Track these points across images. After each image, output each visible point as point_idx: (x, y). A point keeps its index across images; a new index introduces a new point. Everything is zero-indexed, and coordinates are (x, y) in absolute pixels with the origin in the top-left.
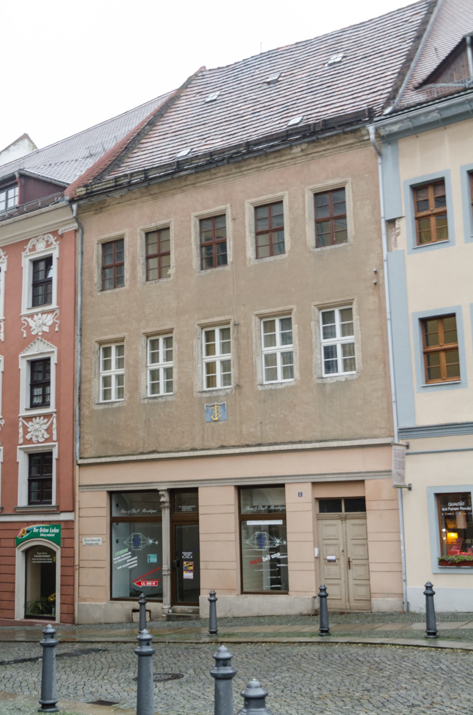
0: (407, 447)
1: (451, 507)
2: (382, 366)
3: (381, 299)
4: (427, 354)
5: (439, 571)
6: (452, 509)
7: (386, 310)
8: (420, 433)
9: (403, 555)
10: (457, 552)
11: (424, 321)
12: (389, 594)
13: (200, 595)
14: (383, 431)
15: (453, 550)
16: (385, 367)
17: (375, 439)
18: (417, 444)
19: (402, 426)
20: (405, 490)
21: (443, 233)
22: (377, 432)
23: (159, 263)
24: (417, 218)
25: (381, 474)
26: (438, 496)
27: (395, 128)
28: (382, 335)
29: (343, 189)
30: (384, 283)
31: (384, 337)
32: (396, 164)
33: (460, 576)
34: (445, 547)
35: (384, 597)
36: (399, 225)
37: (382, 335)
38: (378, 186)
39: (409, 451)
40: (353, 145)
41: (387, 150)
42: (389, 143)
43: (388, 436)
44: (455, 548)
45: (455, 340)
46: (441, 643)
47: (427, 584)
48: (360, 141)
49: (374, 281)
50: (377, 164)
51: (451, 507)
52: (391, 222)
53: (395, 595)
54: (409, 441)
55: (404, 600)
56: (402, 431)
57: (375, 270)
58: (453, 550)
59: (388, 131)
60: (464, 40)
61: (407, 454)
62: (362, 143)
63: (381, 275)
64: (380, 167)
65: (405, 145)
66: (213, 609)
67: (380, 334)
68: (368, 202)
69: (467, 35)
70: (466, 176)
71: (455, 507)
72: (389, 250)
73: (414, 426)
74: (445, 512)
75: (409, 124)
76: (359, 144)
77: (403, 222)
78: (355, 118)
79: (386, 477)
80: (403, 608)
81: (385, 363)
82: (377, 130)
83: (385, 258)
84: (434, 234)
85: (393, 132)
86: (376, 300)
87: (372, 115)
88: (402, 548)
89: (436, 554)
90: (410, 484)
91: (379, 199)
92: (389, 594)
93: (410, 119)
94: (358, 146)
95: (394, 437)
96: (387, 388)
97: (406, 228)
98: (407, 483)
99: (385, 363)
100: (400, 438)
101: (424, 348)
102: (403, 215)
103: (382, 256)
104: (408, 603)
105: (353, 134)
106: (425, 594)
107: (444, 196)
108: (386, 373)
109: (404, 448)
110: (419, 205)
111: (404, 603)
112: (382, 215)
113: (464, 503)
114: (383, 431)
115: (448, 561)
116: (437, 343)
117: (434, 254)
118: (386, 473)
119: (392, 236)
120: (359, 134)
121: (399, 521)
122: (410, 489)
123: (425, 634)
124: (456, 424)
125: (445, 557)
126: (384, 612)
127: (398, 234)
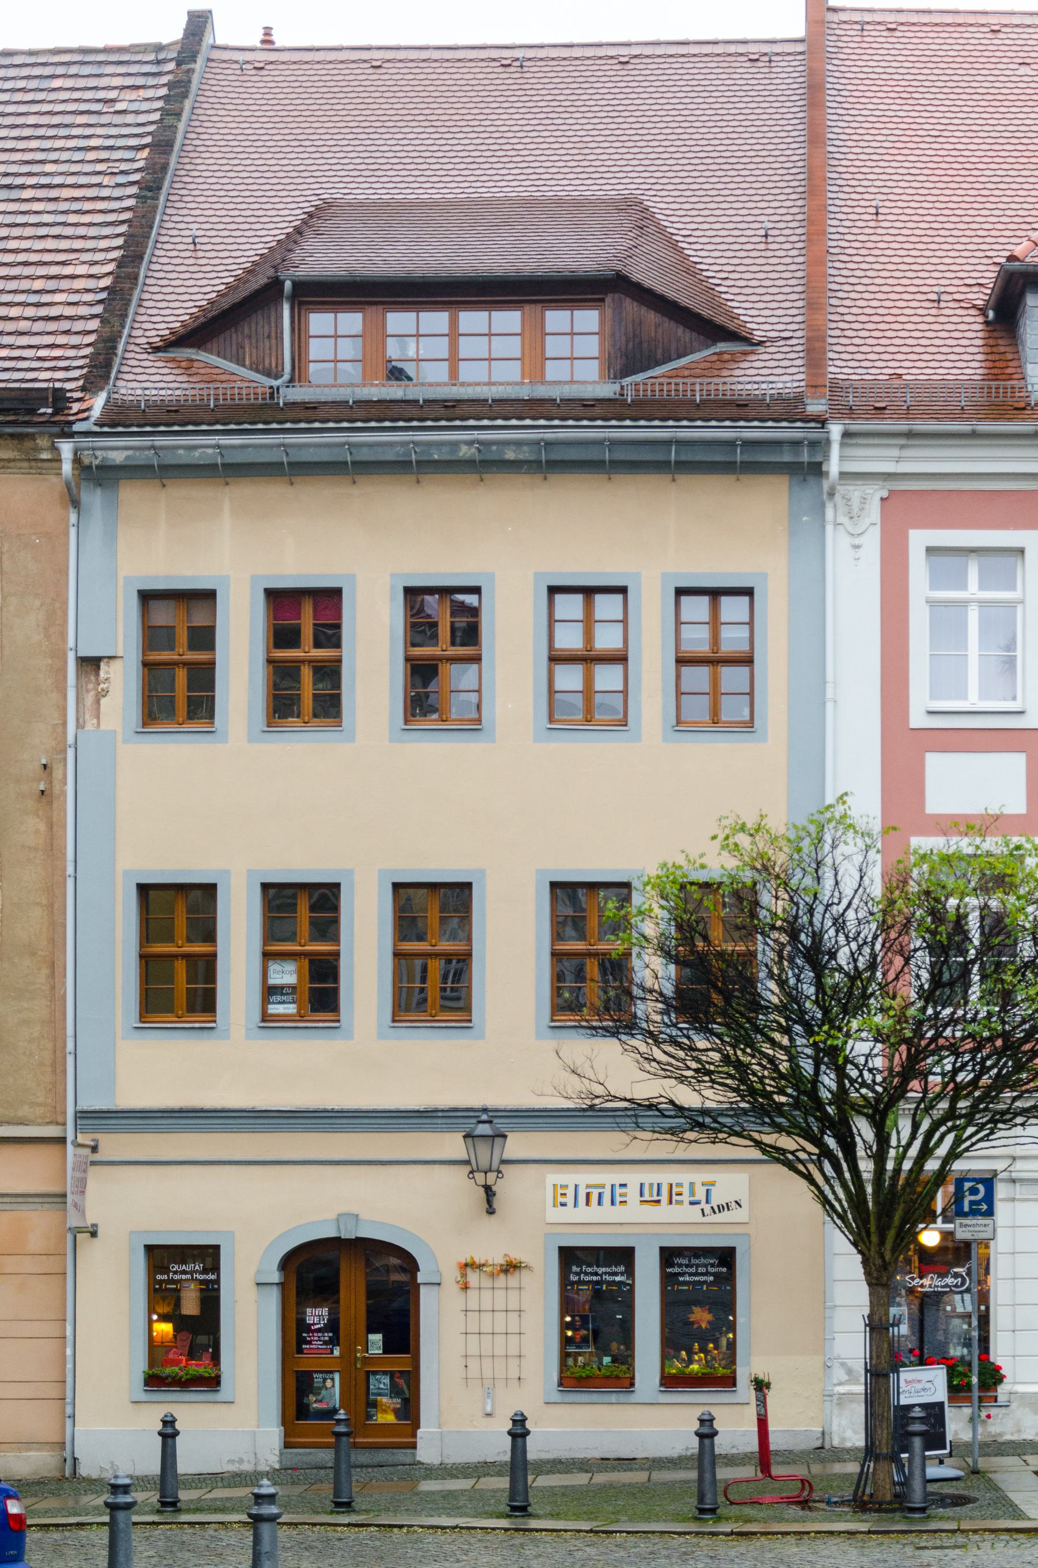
0: (94, 1149)
1: (175, 1273)
2: (45, 971)
3: (53, 829)
4: (146, 959)
5: (144, 1397)
6: (177, 1277)
7: (65, 854)
8: (123, 1122)
9: (69, 1366)
10: (181, 1361)
11: (144, 889)
12: (29, 1445)
14: (39, 1111)
15: (171, 1356)
16: (52, 975)
17: (21, 1127)
18: (115, 1144)
19: (85, 1105)
22: (24, 1111)
24: (145, 664)
25: (30, 1200)
26: (150, 1249)
28: (51, 905)
30: (64, 793)
31: (54, 910)
32: (111, 538)
33: (187, 1405)
34: (155, 1348)
35: (20, 1450)
36: (107, 672)
37: (51, 905)
39: (97, 1157)
40: (12, 464)
41: (93, 498)
42: (99, 484)
43: (48, 1123)
44: (175, 1353)
45: (210, 936)
47: (166, 1416)
48: (29, 460)
49: (42, 787)
51: (175, 1273)
52: (90, 664)
53: (42, 1445)
54: (98, 1136)
55: (67, 1454)
56: (82, 1115)
57: (44, 761)
58: (171, 1356)
59: (100, 458)
61: (93, 1163)
62: (33, 464)
63: (57, 774)
64: (73, 531)
65: (132, 495)
67: (45, 902)
68: (37, 603)
70: (261, 597)
71: (184, 1272)
72: (80, 725)
73: (112, 1107)
74: (161, 1282)
76: (26, 464)
77: (116, 667)
78: (22, 401)
79: (39, 1206)
80: (64, 1470)
81: (52, 965)
83: (70, 739)
85: (110, 463)
86: (42, 827)
87: (60, 405)
88: (69, 1352)
89: (141, 1365)
90: (94, 1225)
91: (66, 602)
92: (29, 1445)
94: (21, 468)
95: (64, 1124)
96: (55, 1022)
97: (122, 682)
98: (89, 1222)
99: (52, 965)
101: (141, 946)
102: (120, 654)
103: (65, 738)
104: (75, 1459)
105: (15, 442)
106: (160, 1434)
107: (211, 630)
108: (53, 988)
109: (88, 1151)
110: (153, 637)
111: (65, 1460)
112: (71, 643)
113: (693, 1318)
114: (39, 1111)
115: (167, 1378)
116: (170, 939)
117: (177, 751)
118: (40, 1200)
119: (88, 691)
120: (28, 444)
121: (65, 1299)
122: (94, 1234)
123: (158, 1506)
124: (202, 1111)
125: (157, 1371)
126: (20, 1481)
127: (105, 693)
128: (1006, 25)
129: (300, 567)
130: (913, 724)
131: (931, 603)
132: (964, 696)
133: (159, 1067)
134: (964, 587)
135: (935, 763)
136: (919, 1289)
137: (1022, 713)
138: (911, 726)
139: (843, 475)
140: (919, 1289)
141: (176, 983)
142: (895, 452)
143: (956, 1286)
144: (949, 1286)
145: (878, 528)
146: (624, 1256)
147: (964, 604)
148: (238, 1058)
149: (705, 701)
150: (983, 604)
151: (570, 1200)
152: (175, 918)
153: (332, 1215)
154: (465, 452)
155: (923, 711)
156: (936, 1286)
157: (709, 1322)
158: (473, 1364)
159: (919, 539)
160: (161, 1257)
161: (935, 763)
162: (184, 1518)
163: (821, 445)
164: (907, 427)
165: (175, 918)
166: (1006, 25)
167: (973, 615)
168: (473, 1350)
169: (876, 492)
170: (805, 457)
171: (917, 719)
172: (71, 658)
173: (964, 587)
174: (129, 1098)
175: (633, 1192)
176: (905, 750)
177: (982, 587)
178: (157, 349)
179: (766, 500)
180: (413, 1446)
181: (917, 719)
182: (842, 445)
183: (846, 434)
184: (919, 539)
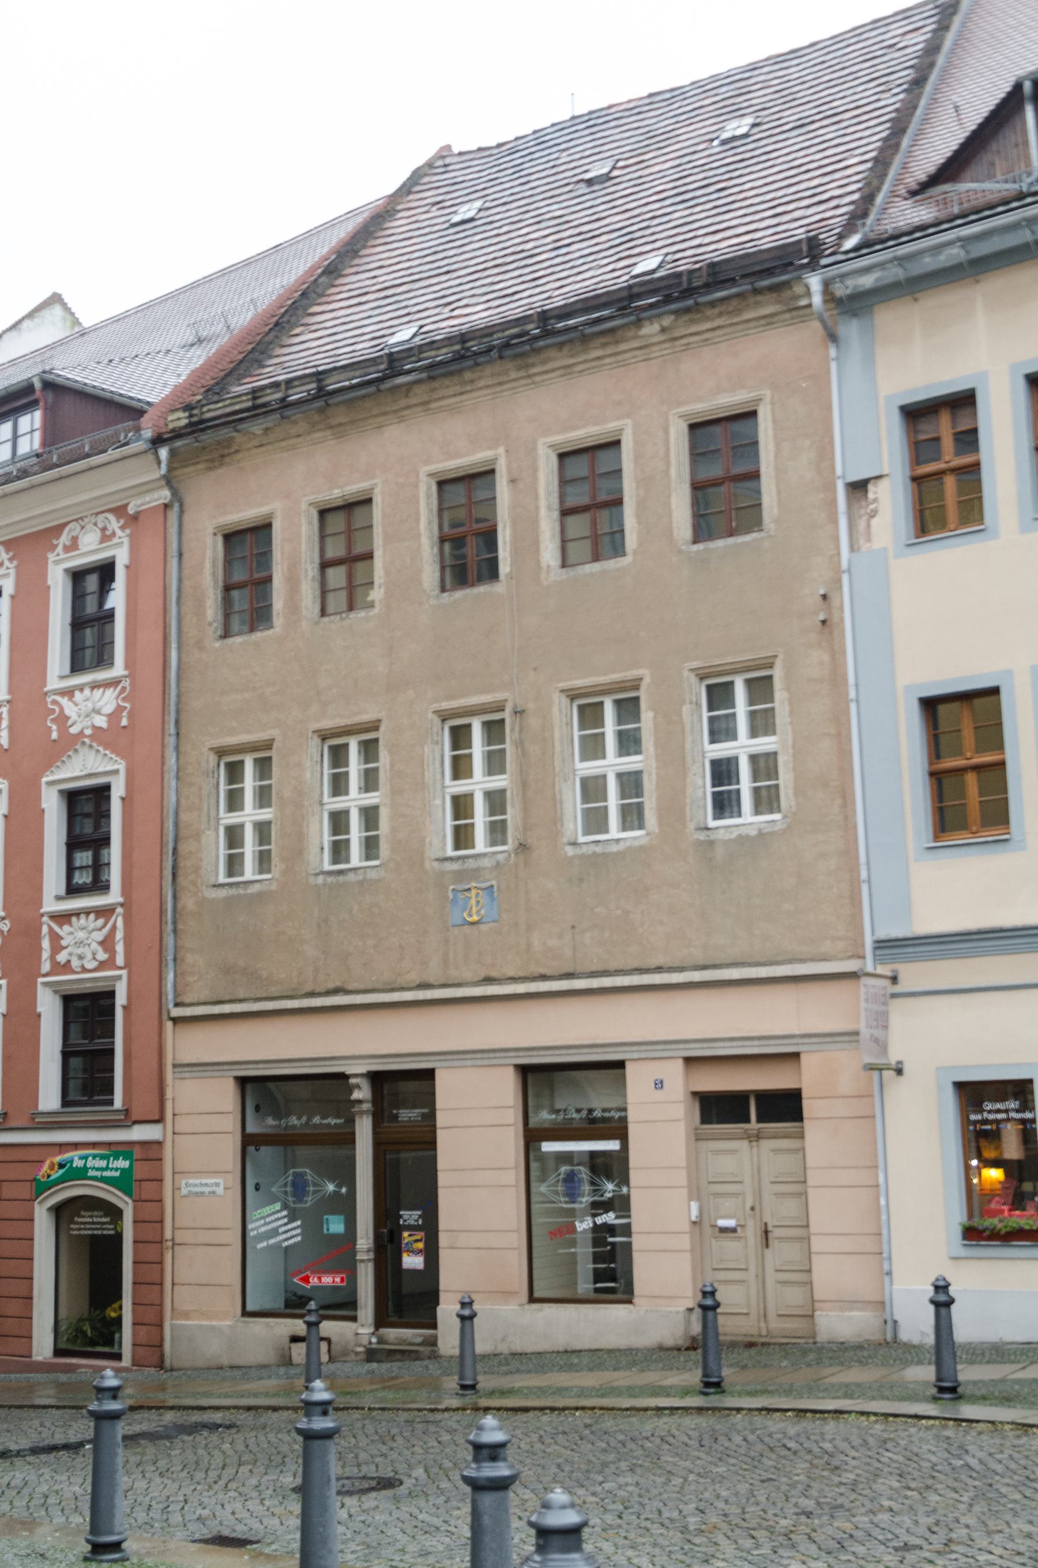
0: (894, 979)
1: (990, 1112)
2: (839, 802)
3: (837, 656)
4: (937, 777)
5: (963, 1252)
6: (991, 1117)
7: (846, 680)
8: (921, 949)
9: (884, 1217)
10: (1002, 1211)
11: (930, 705)
12: (853, 1304)
14: (840, 945)
15: (993, 1206)
16: (844, 805)
17: (823, 963)
18: (915, 974)
19: (883, 934)
20: (888, 1075)
21: (972, 511)
22: (827, 947)
23: (350, 577)
24: (915, 479)
25: (837, 1039)
26: (961, 1087)
27: (867, 281)
28: (839, 734)
29: (753, 414)
30: (842, 620)
31: (842, 739)
32: (869, 361)
33: (1010, 1262)
34: (976, 1199)
35: (842, 1309)
36: (876, 493)
37: (839, 734)
38: (829, 408)
39: (897, 989)
40: (776, 319)
41: (850, 329)
42: (854, 314)
43: (851, 957)
44: (998, 1202)
45: (999, 745)
47: (937, 1280)
48: (790, 310)
49: (822, 617)
50: (827, 360)
51: (990, 1112)
52: (859, 488)
53: (866, 1304)
54: (898, 966)
55: (888, 1317)
56: (881, 945)
57: (822, 592)
58: (993, 1206)
59: (851, 287)
60: (1018, 87)
61: (894, 996)
62: (794, 313)
63: (835, 602)
64: (833, 366)
65: (888, 318)
67: (833, 731)
68: (808, 442)
69: (1025, 78)
70: (1022, 385)
71: (998, 1111)
72: (853, 548)
73: (909, 934)
74: (975, 1122)
75: (897, 273)
76: (787, 316)
77: (883, 486)
78: (780, 258)
79: (847, 1046)
80: (885, 1334)
81: (844, 797)
82: (827, 284)
83: (844, 565)
84: (952, 512)
85: (861, 289)
86: (826, 657)
87: (816, 252)
88: (883, 1202)
89: (958, 1216)
90: (900, 1063)
91: (832, 437)
92: (853, 1304)
93: (900, 260)
94: (785, 321)
95: (864, 957)
96: (850, 852)
97: (892, 500)
98: (893, 1059)
99: (844, 797)
100: (877, 960)
101: (931, 764)
102: (885, 472)
103: (839, 562)
104: (895, 1322)
105: (774, 295)
106: (932, 1302)
107: (975, 431)
108: (846, 818)
109: (887, 983)
110: (920, 450)
111: (886, 1322)
112: (839, 471)
114: (840, 945)
115: (984, 1231)
116: (959, 752)
117: (951, 556)
118: (847, 1038)
119: (860, 517)
120: (787, 294)
121: (875, 1142)
122: (899, 1072)
123: (934, 1391)
124: (1002, 930)
125: (977, 1222)
126: (842, 1343)
127: (873, 514)
162: (968, 1411)
178: (913, 193)
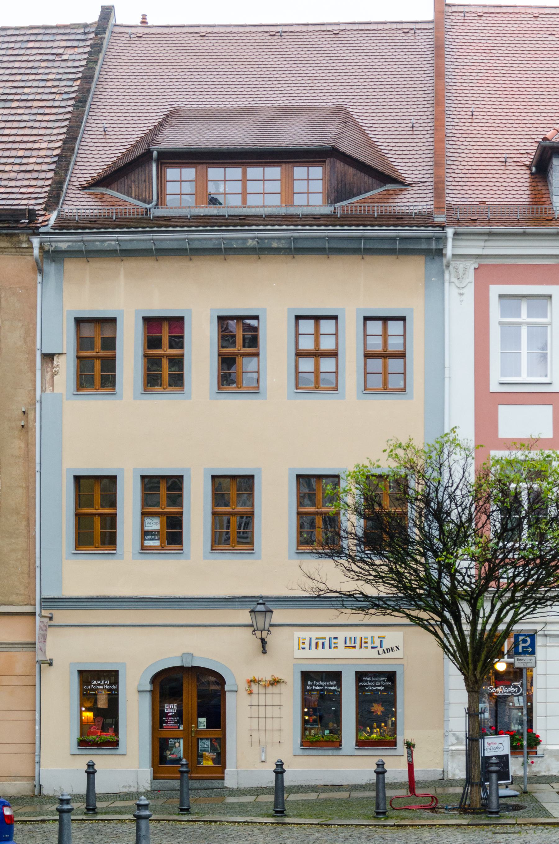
0: (51, 618)
1: (94, 685)
2: (24, 523)
3: (29, 446)
4: (79, 516)
5: (77, 752)
6: (95, 687)
7: (35, 460)
8: (66, 604)
9: (37, 735)
10: (97, 733)
11: (77, 479)
12: (16, 778)
13: (225, 768)
14: (21, 598)
15: (92, 730)
16: (28, 525)
17: (11, 607)
18: (62, 616)
19: (46, 595)
22: (13, 598)
24: (78, 357)
25: (16, 646)
26: (81, 672)
28: (28, 487)
30: (34, 427)
31: (29, 490)
32: (60, 289)
33: (101, 756)
34: (83, 725)
35: (11, 781)
36: (58, 362)
37: (28, 487)
39: (52, 623)
40: (6, 250)
41: (50, 268)
42: (53, 260)
43: (26, 605)
44: (94, 728)
45: (113, 504)
46: (99, 817)
47: (89, 762)
48: (16, 248)
49: (23, 424)
51: (94, 685)
52: (49, 357)
53: (23, 778)
54: (53, 612)
55: (36, 783)
56: (44, 600)
57: (24, 410)
58: (92, 730)
59: (54, 247)
61: (50, 626)
62: (18, 250)
63: (31, 416)
64: (39, 286)
65: (71, 267)
66: (91, 780)
67: (24, 485)
68: (20, 324)
70: (141, 321)
71: (99, 685)
72: (43, 390)
73: (60, 596)
74: (87, 690)
76: (14, 250)
77: (62, 359)
78: (12, 216)
79: (21, 649)
80: (34, 791)
81: (28, 520)
83: (38, 398)
85: (59, 249)
86: (23, 445)
87: (32, 218)
88: (37, 727)
89: (76, 735)
90: (51, 660)
91: (35, 324)
92: (16, 778)
94: (11, 252)
95: (35, 605)
96: (30, 550)
97: (66, 367)
98: (48, 658)
99: (28, 520)
101: (76, 509)
102: (65, 352)
103: (35, 397)
104: (40, 785)
105: (8, 238)
107: (114, 339)
108: (29, 532)
109: (47, 619)
110: (82, 343)
111: (35, 786)
112: (38, 346)
114: (21, 598)
115: (90, 742)
116: (92, 505)
117: (95, 404)
118: (22, 646)
119: (47, 372)
120: (15, 239)
121: (35, 699)
122: (50, 664)
123: (85, 810)
124: (109, 598)
125: (84, 738)
126: (11, 797)
127: (57, 373)
128: (542, 14)
129: (161, 305)
130: (492, 390)
131: (502, 324)
132: (519, 375)
133: (86, 574)
134: (519, 316)
135: (504, 411)
136: (495, 694)
137: (550, 384)
138: (491, 391)
139: (454, 256)
140: (495, 694)
141: (95, 529)
142: (482, 243)
143: (515, 692)
144: (511, 692)
145: (473, 284)
146: (336, 676)
147: (519, 325)
148: (128, 569)
149: (380, 377)
150: (529, 325)
151: (307, 646)
152: (94, 494)
153: (179, 654)
154: (250, 243)
155: (497, 383)
156: (504, 692)
157: (382, 712)
158: (255, 734)
159: (495, 290)
160: (87, 677)
161: (504, 411)
163: (442, 240)
164: (488, 230)
165: (94, 494)
166: (542, 14)
167: (524, 331)
168: (255, 727)
169: (472, 265)
170: (434, 246)
171: (494, 387)
172: (38, 354)
173: (519, 316)
174: (69, 591)
175: (341, 642)
176: (487, 404)
177: (529, 316)
178: (84, 188)
179: (412, 269)
180: (223, 778)
181: (494, 387)
182: (454, 239)
183: (456, 234)
184: (495, 290)
